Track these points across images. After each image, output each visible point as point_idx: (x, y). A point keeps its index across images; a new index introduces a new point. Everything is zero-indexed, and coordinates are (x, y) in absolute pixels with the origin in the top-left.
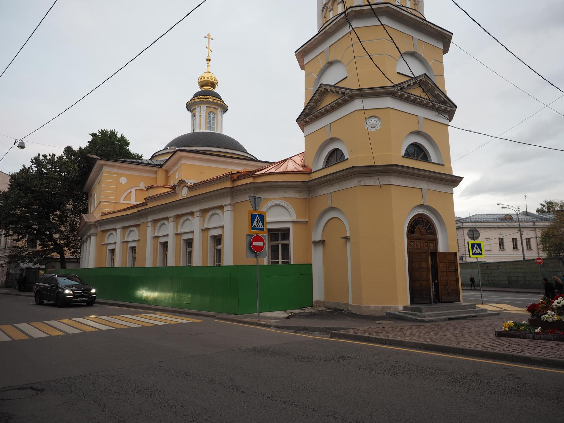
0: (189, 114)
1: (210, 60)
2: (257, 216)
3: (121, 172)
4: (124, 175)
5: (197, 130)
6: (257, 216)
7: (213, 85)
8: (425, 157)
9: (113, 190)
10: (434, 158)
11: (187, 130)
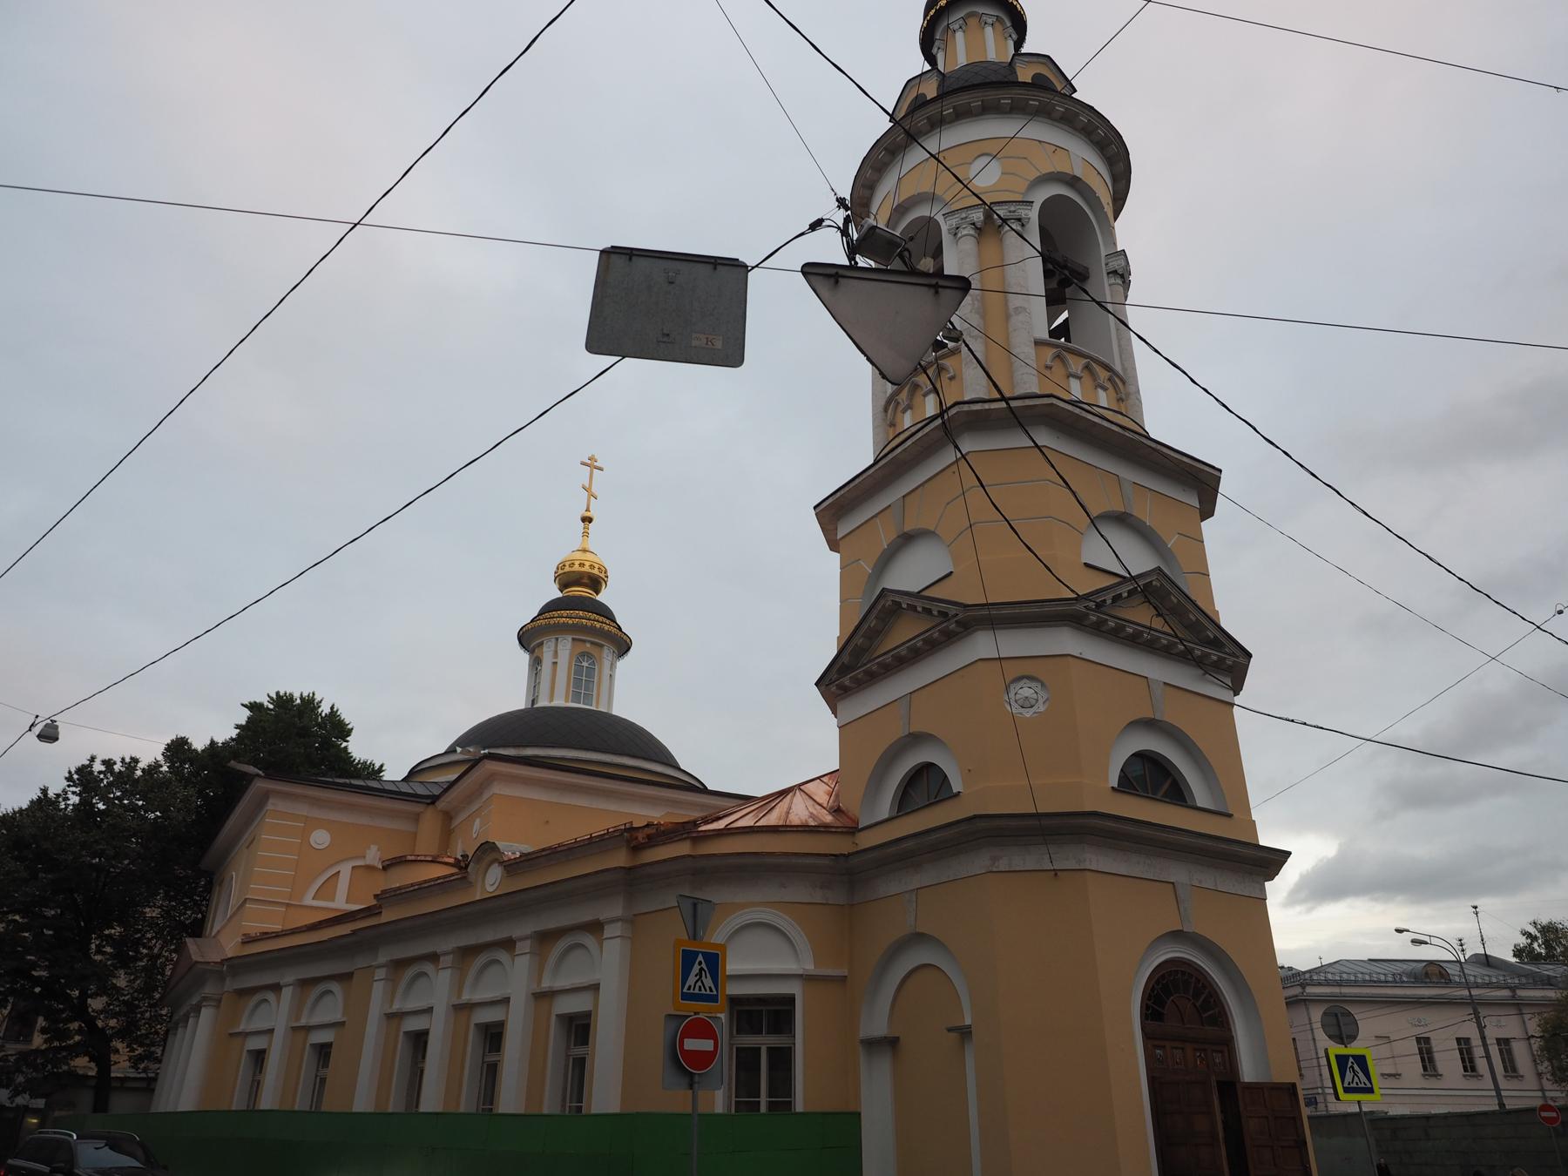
0: (524, 658)
1: (590, 520)
2: (700, 958)
3: (316, 813)
4: (320, 824)
5: (543, 703)
6: (700, 958)
7: (596, 583)
8: (1177, 793)
9: (291, 870)
10: (1201, 798)
11: (515, 700)
